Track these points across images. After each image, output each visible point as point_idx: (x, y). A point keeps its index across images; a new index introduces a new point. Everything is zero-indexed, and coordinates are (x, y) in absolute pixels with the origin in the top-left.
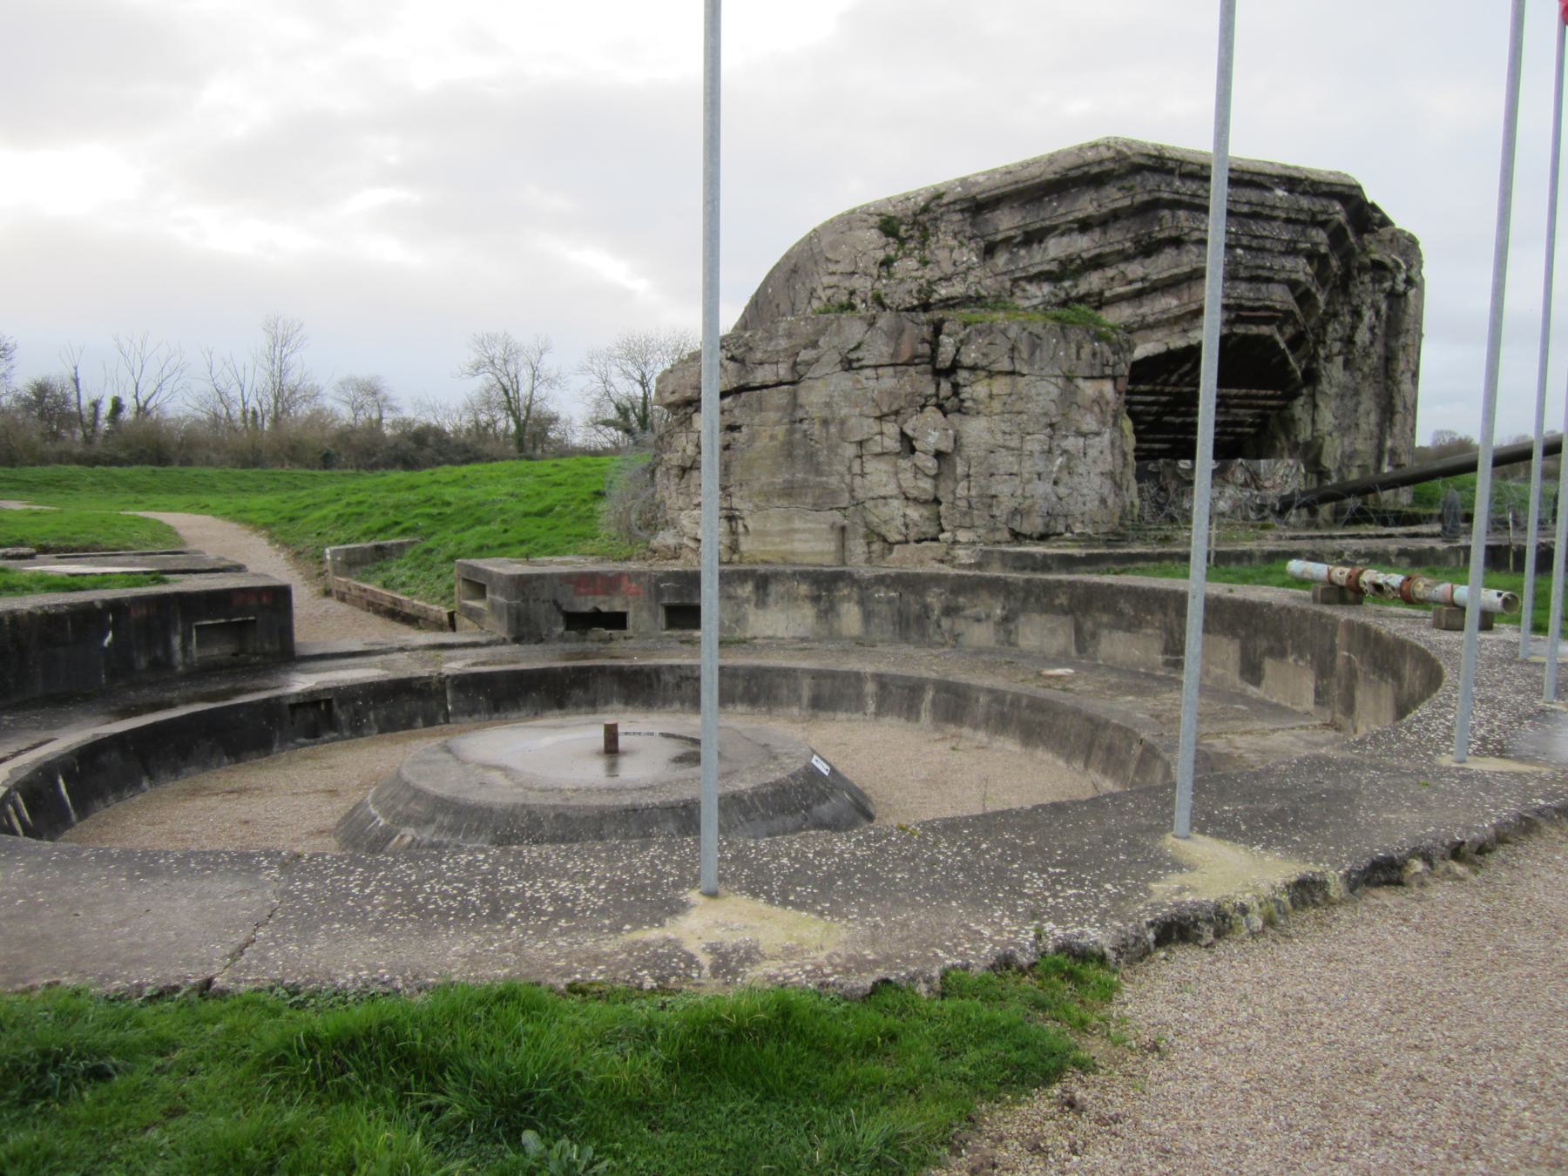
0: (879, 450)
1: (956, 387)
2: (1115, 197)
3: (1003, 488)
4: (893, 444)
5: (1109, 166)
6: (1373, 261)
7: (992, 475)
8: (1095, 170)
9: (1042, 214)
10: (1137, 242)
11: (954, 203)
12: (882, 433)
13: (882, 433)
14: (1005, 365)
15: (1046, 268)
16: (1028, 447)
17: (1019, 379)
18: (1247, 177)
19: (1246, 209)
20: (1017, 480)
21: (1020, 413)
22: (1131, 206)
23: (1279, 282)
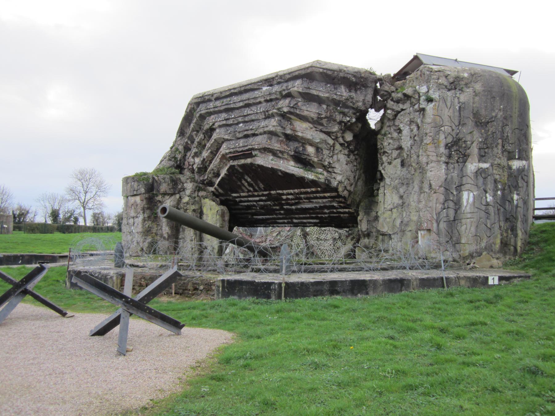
19: (241, 104)
23: (261, 134)
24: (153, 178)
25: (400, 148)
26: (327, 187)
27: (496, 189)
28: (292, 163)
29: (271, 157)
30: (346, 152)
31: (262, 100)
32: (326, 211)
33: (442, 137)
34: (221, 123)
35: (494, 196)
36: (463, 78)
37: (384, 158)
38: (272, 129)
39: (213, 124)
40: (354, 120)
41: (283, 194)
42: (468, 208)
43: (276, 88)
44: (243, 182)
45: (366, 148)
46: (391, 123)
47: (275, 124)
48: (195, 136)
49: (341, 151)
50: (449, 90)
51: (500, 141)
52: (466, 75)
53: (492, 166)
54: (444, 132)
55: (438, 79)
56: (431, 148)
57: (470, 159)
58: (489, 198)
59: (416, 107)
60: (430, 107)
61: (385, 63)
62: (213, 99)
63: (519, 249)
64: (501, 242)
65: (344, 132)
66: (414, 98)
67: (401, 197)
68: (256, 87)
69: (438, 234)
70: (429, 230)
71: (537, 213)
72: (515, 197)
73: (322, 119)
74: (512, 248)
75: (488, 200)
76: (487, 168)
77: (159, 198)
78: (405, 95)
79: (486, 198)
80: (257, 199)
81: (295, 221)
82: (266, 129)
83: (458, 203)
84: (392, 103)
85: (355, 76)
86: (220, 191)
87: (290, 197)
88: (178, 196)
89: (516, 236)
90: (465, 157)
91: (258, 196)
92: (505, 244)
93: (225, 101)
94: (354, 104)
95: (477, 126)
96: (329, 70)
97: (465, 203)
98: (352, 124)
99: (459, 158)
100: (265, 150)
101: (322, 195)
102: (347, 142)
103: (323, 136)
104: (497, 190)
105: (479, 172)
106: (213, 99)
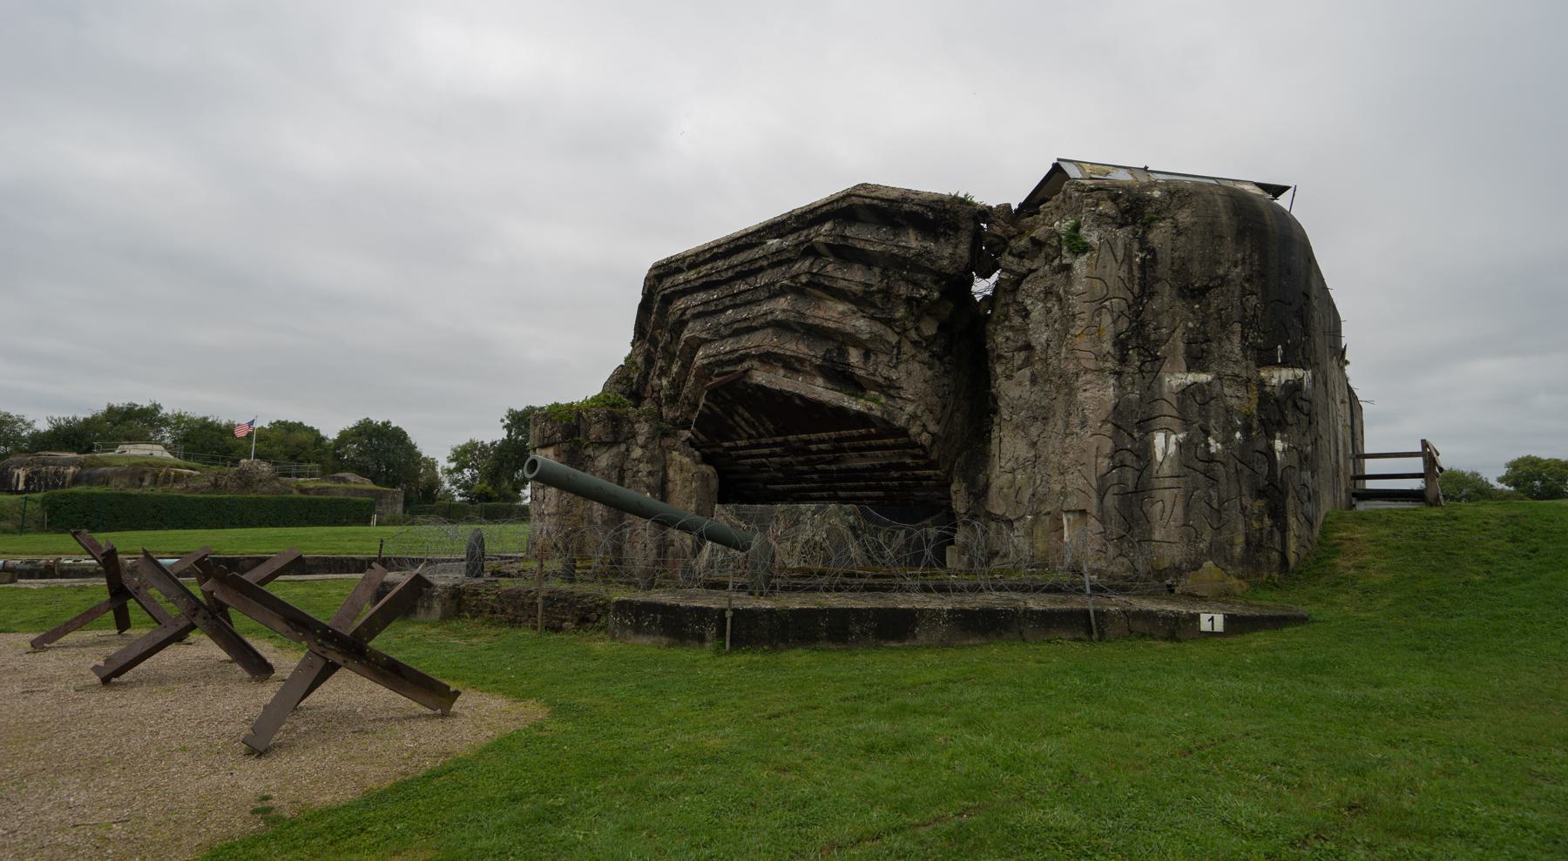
24: (579, 415)
25: (1028, 347)
26: (887, 428)
27: (1228, 429)
28: (820, 381)
29: (782, 372)
30: (925, 356)
31: (765, 263)
32: (894, 474)
33: (1107, 320)
35: (1227, 441)
36: (1151, 200)
37: (999, 370)
38: (780, 316)
39: (683, 314)
40: (936, 295)
41: (810, 442)
42: (1165, 466)
43: (789, 241)
44: (737, 418)
45: (965, 346)
46: (1009, 299)
47: (785, 306)
49: (914, 356)
50: (1121, 226)
51: (1237, 327)
52: (1156, 194)
53: (1219, 377)
54: (1111, 312)
55: (1097, 205)
56: (1083, 343)
57: (1167, 365)
58: (1215, 447)
59: (1056, 262)
60: (1080, 265)
61: (1002, 183)
62: (684, 266)
63: (1292, 558)
64: (1248, 542)
65: (918, 320)
67: (1034, 445)
68: (754, 240)
69: (1102, 521)
70: (1083, 512)
71: (1370, 485)
72: (1279, 445)
73: (872, 294)
74: (1275, 556)
75: (1213, 450)
76: (1209, 384)
77: (590, 451)
78: (1033, 240)
79: (1208, 445)
80: (767, 451)
81: (841, 494)
83: (1144, 454)
84: (1010, 258)
85: (932, 209)
86: (701, 436)
87: (823, 446)
88: (623, 447)
89: (1284, 529)
90: (1153, 360)
91: (767, 446)
92: (1255, 546)
93: (704, 270)
94: (933, 262)
95: (1184, 297)
96: (882, 200)
97: (1159, 457)
98: (933, 303)
99: (1143, 363)
100: (767, 358)
101: (879, 442)
102: (926, 339)
103: (878, 328)
104: (1234, 431)
105: (1186, 392)
106: (684, 266)
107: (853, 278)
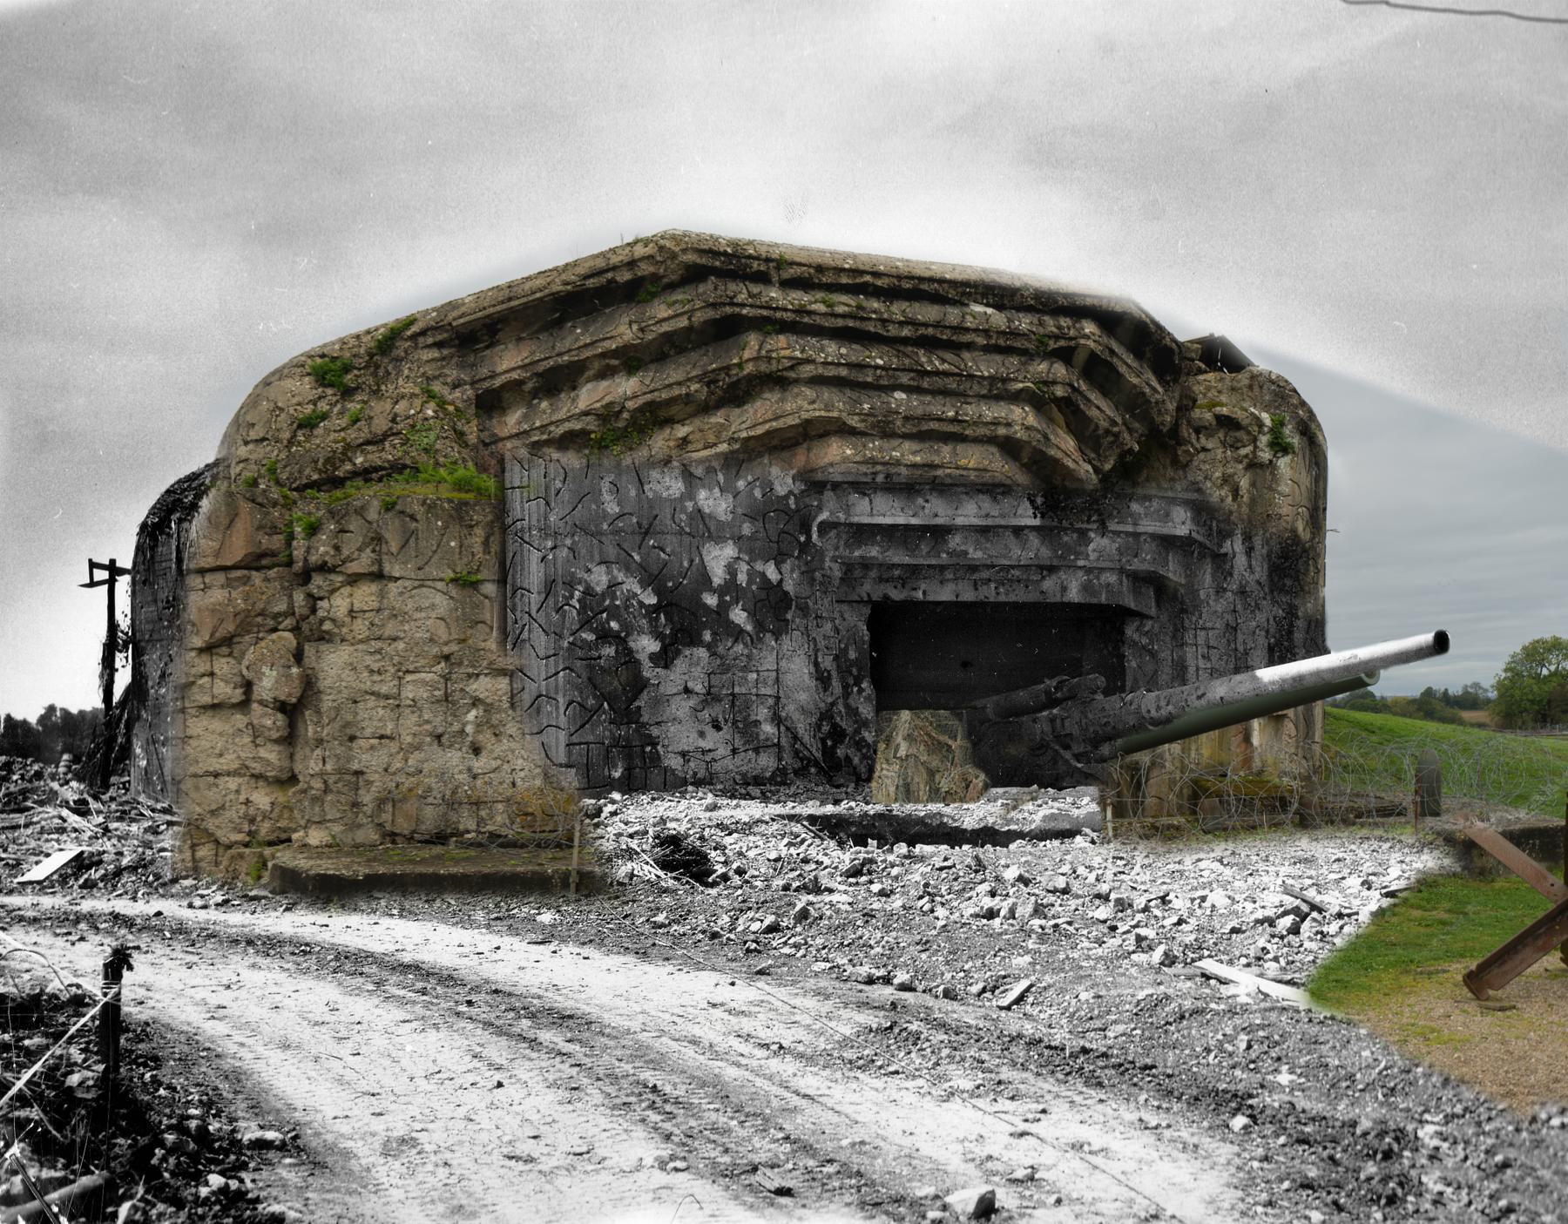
0: (207, 700)
1: (313, 599)
2: (664, 314)
3: (368, 758)
4: (225, 690)
5: (646, 269)
6: (1218, 417)
7: (352, 738)
8: (625, 276)
9: (559, 347)
10: (709, 380)
11: (423, 333)
12: (212, 674)
13: (212, 674)
14: (363, 563)
15: (577, 426)
16: (409, 693)
17: (391, 585)
18: (907, 285)
20: (394, 747)
21: (395, 639)
22: (690, 329)
23: (977, 440)
34: (831, 372)
48: (591, 373)
66: (1249, 433)
82: (1002, 431)
107: (1101, 409)
